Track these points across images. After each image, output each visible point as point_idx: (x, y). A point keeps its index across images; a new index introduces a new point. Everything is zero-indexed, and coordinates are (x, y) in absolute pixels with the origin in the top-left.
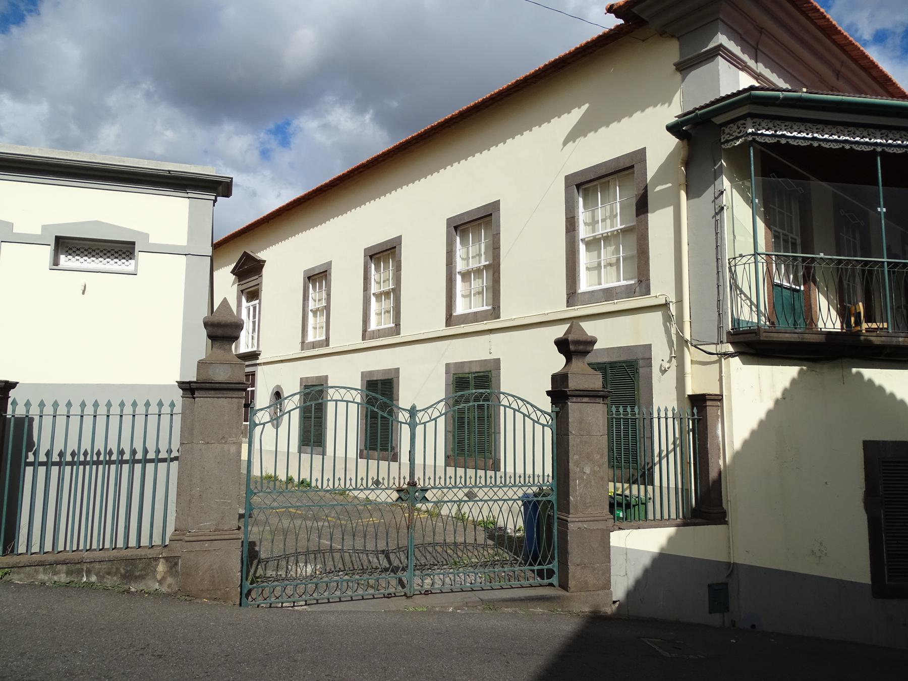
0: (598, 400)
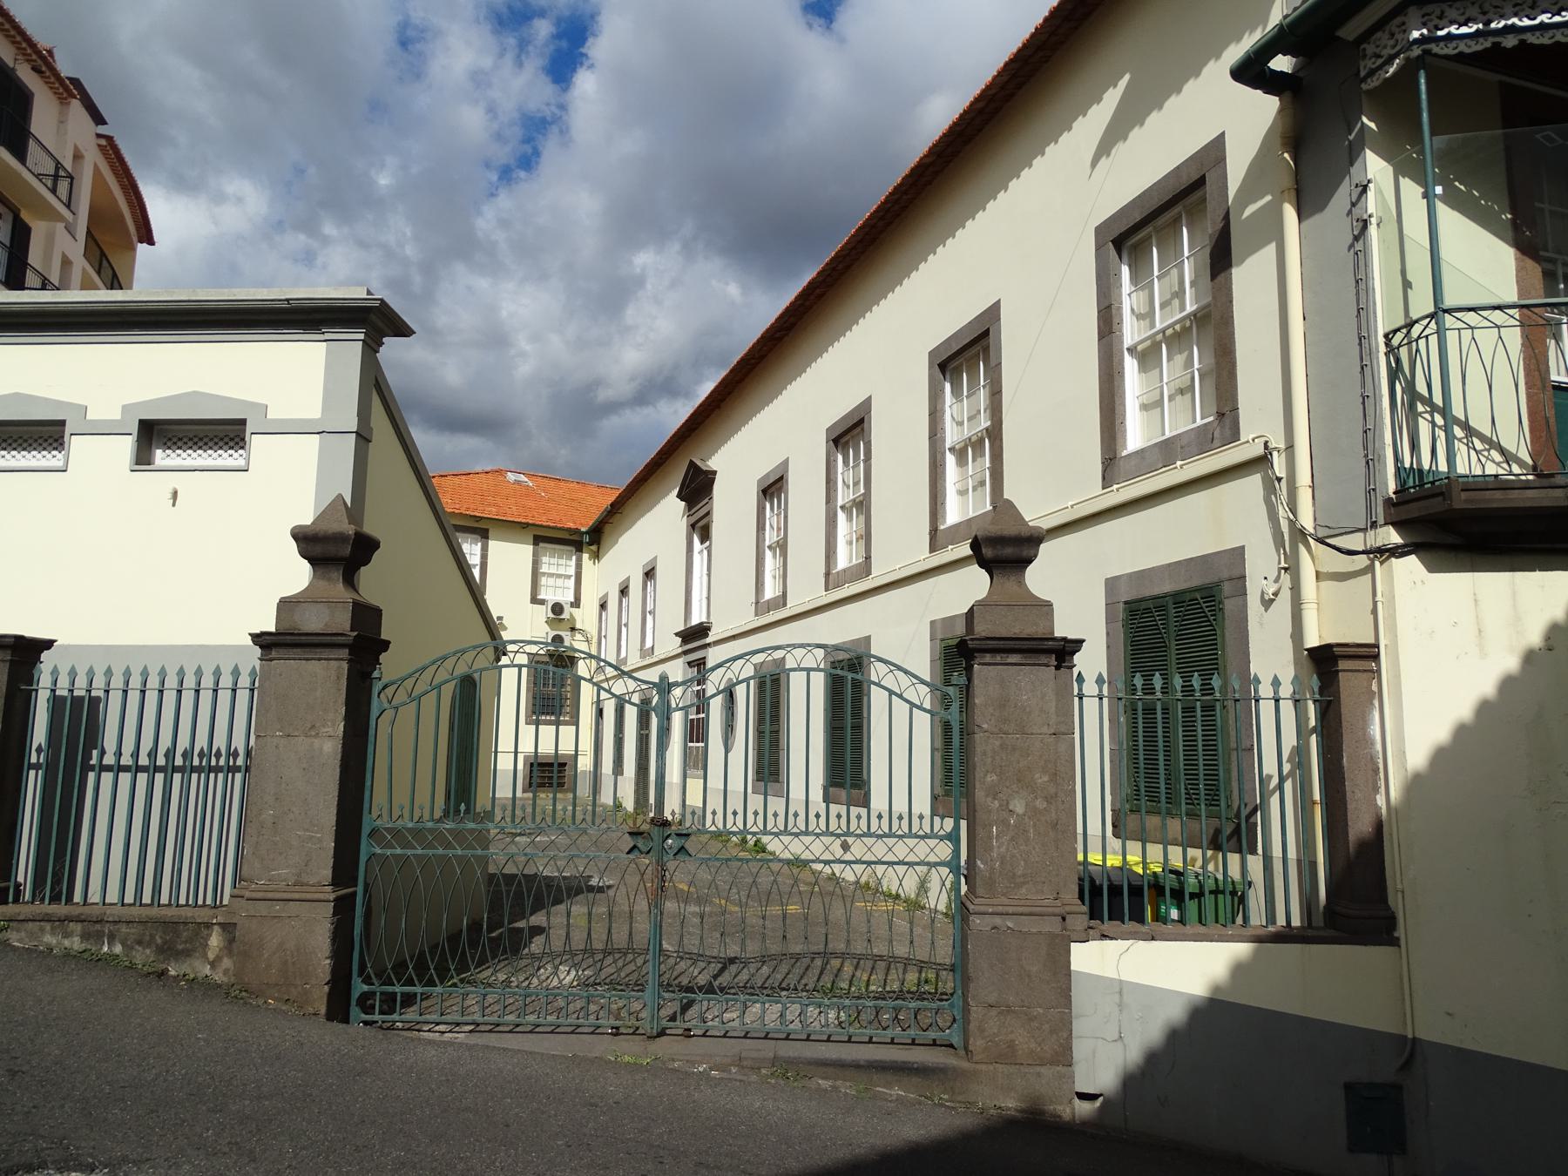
0: (1043, 659)
